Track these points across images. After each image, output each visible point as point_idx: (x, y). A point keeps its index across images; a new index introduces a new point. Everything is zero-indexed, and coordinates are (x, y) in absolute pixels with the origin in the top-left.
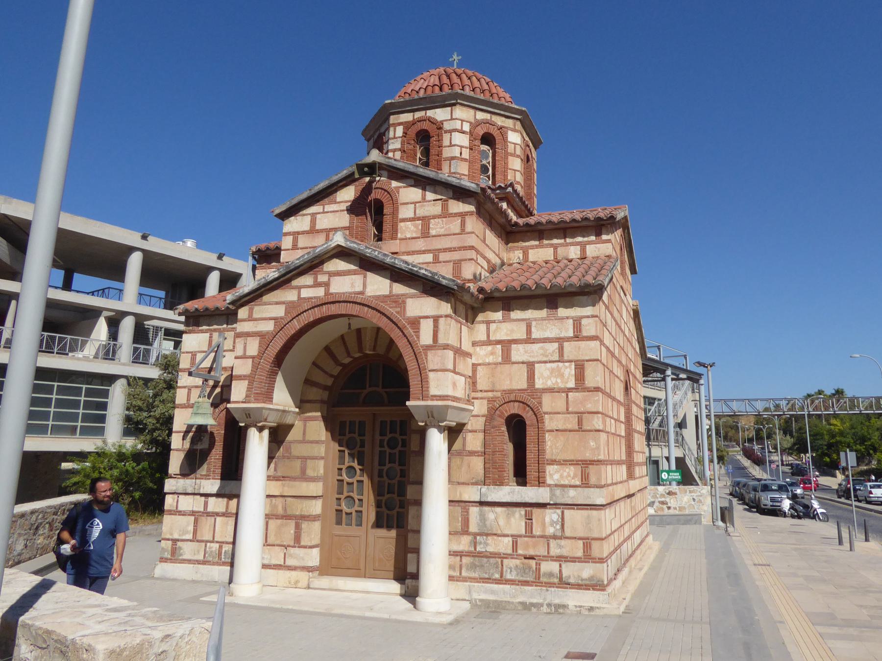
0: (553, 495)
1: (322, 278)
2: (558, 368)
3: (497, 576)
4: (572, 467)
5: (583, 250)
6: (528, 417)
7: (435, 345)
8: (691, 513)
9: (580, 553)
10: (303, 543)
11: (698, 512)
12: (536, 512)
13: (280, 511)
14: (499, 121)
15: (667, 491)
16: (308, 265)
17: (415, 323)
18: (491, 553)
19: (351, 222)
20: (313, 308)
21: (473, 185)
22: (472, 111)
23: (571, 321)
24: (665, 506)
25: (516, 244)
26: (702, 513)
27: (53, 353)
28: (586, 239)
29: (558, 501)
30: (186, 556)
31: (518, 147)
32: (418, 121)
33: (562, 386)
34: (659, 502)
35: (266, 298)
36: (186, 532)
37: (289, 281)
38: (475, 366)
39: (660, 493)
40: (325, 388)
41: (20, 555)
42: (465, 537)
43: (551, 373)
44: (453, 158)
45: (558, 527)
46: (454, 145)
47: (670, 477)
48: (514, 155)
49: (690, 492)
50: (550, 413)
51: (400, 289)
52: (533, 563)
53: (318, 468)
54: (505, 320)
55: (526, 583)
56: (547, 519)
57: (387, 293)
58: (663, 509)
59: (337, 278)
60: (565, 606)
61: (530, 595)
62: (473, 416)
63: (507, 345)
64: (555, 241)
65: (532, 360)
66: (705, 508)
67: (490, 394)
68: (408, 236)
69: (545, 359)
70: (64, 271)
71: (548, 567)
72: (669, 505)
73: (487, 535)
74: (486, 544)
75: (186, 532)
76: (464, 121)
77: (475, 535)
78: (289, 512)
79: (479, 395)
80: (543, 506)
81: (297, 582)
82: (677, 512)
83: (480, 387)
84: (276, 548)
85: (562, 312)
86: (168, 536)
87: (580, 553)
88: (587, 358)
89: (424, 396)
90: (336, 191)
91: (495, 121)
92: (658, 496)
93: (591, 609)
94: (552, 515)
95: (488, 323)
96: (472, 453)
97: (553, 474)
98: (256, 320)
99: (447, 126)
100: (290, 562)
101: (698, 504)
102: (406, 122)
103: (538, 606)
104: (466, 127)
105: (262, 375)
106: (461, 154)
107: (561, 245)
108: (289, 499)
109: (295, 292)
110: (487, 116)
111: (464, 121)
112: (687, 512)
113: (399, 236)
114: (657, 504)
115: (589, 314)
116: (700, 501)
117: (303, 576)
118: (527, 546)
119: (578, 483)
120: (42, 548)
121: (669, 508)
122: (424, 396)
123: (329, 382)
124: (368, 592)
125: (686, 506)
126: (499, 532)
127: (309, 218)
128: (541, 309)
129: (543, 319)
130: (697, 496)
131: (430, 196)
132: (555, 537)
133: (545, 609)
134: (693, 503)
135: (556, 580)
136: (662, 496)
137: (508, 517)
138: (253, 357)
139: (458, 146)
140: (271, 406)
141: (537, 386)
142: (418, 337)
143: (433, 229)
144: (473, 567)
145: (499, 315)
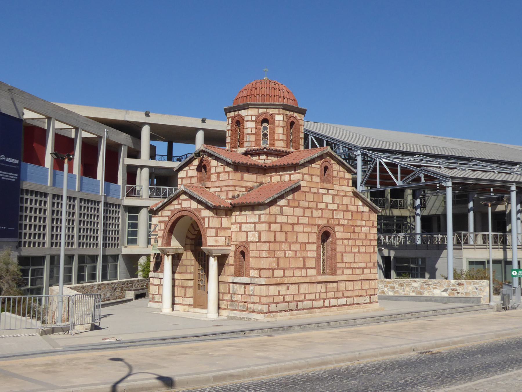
0: (251, 280)
1: (180, 201)
2: (254, 234)
3: (237, 308)
4: (257, 270)
5: (290, 177)
6: (246, 251)
7: (208, 228)
8: (473, 296)
9: (258, 301)
10: (187, 296)
11: (479, 296)
12: (247, 286)
13: (180, 285)
14: (271, 111)
15: (457, 283)
16: (175, 197)
17: (204, 219)
18: (236, 301)
19: (197, 174)
20: (178, 212)
21: (230, 161)
22: (256, 110)
23: (258, 216)
24: (455, 292)
25: (268, 174)
26: (482, 297)
27: (160, 198)
28: (291, 172)
29: (253, 283)
30: (156, 300)
31: (281, 122)
32: (236, 116)
33: (255, 240)
34: (451, 289)
35: (166, 208)
36: (156, 292)
37: (171, 202)
38: (232, 232)
39: (452, 284)
40: (192, 239)
41: (109, 297)
42: (229, 294)
43: (252, 235)
44: (248, 134)
45: (253, 292)
46: (248, 128)
47: (520, 274)
48: (279, 126)
49: (474, 284)
50: (252, 251)
51: (200, 206)
52: (246, 304)
53: (192, 269)
54: (240, 215)
55: (244, 311)
56: (250, 289)
57: (196, 208)
58: (454, 294)
59: (184, 201)
60: (250, 319)
61: (244, 315)
62: (232, 251)
63: (240, 224)
64: (281, 173)
65: (247, 230)
66: (485, 294)
67: (236, 243)
68: (214, 180)
69: (251, 230)
70: (167, 143)
71: (250, 305)
72: (458, 291)
73: (235, 294)
74: (234, 297)
75: (156, 292)
76: (253, 115)
77: (232, 294)
78: (183, 285)
79: (233, 243)
80: (249, 284)
81: (185, 309)
82: (464, 296)
83: (233, 240)
84: (180, 297)
85: (256, 212)
86: (151, 293)
87: (258, 301)
88: (262, 230)
89: (206, 246)
90: (193, 161)
91: (269, 112)
92: (450, 285)
93: (257, 320)
94: (251, 287)
95: (236, 216)
96: (231, 265)
97: (253, 273)
98: (163, 216)
99: (246, 119)
100: (184, 303)
101: (479, 291)
102: (232, 117)
103: (244, 318)
104: (254, 118)
105: (165, 237)
106: (251, 131)
107: (283, 175)
108: (182, 280)
109: (173, 206)
110: (265, 110)
111: (253, 115)
112: (471, 296)
113: (211, 180)
114: (449, 291)
115: (263, 213)
116: (481, 290)
117: (186, 307)
118: (244, 299)
119: (258, 276)
120: (119, 296)
121: (458, 293)
122: (206, 246)
123: (194, 237)
124: (203, 313)
125: (470, 292)
126: (237, 293)
127: (185, 172)
128: (250, 211)
129: (251, 215)
130: (479, 286)
131: (220, 164)
132: (252, 295)
133: (246, 319)
134: (476, 290)
135: (252, 310)
136: (454, 285)
137: (240, 287)
138: (163, 230)
139: (249, 128)
140: (170, 247)
141: (248, 240)
142: (204, 224)
143: (221, 177)
144: (231, 305)
145: (238, 213)
